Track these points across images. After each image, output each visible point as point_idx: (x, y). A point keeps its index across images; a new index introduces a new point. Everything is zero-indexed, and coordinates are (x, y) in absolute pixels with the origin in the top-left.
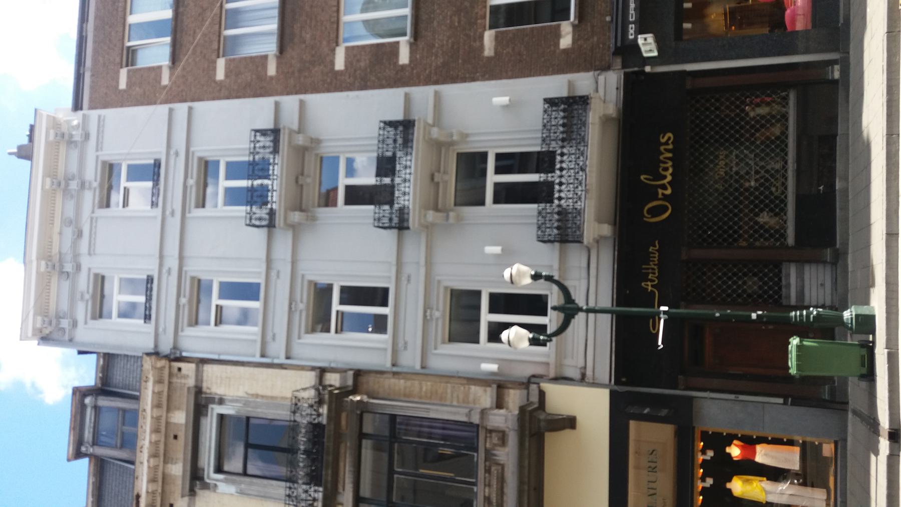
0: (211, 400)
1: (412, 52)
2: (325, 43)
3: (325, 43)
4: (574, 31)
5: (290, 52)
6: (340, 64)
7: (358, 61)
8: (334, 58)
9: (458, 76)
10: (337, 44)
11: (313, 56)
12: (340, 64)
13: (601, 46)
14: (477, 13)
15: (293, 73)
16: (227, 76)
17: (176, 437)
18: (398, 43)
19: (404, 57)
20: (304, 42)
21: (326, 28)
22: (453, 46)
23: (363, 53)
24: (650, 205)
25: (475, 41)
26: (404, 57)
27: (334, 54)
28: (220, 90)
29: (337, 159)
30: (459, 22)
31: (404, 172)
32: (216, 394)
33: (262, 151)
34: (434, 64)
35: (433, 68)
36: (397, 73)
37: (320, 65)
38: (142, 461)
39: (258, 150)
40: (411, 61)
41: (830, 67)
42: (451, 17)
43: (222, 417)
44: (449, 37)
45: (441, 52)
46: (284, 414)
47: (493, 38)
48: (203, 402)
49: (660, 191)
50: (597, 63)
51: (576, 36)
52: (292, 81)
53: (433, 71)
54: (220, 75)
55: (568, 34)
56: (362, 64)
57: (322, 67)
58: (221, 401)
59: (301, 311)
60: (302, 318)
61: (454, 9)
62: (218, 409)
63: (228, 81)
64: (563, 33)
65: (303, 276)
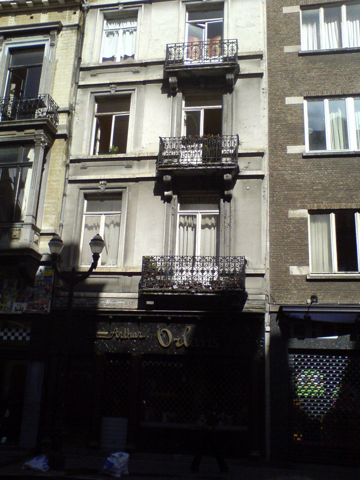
0: (53, 38)
1: (295, 155)
2: (307, 87)
3: (307, 87)
4: (303, 276)
5: (302, 59)
6: (290, 100)
7: (292, 114)
8: (295, 96)
9: (275, 191)
10: (306, 98)
11: (297, 80)
12: (290, 100)
13: (289, 296)
14: (322, 203)
15: (285, 66)
16: (285, 15)
17: (32, 18)
18: (304, 144)
19: (292, 149)
20: (309, 72)
21: (318, 87)
22: (298, 186)
23: (297, 118)
24: (169, 332)
25: (301, 203)
26: (292, 149)
27: (298, 96)
28: (275, 11)
29: (221, 103)
30: (317, 190)
31: (189, 157)
32: (57, 41)
33: (230, 48)
34: (285, 172)
35: (283, 172)
36: (280, 145)
37: (291, 85)
38: (107, 228)
39: (231, 45)
40: (289, 155)
41: (49, 111)
42: (320, 183)
43: (42, 47)
44: (305, 182)
45: (294, 177)
46: (42, 91)
47: (302, 216)
48: (51, 33)
49: (178, 339)
50: (277, 294)
51: (298, 278)
52: (278, 65)
53: (280, 172)
54: (286, 10)
55: (301, 272)
56: (289, 118)
57: (288, 87)
58: (52, 45)
59: (110, 92)
60: (104, 92)
61: (327, 185)
62: (47, 44)
63: (282, 16)
64: (301, 268)
65: (134, 90)
